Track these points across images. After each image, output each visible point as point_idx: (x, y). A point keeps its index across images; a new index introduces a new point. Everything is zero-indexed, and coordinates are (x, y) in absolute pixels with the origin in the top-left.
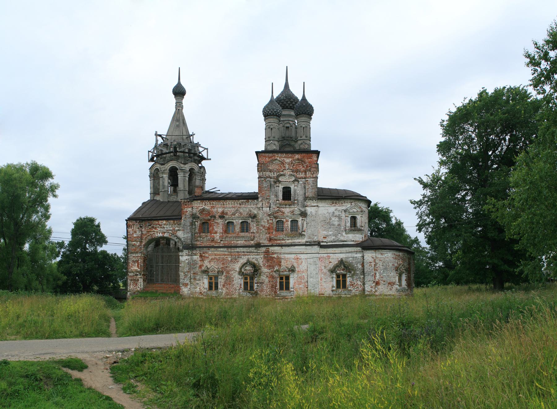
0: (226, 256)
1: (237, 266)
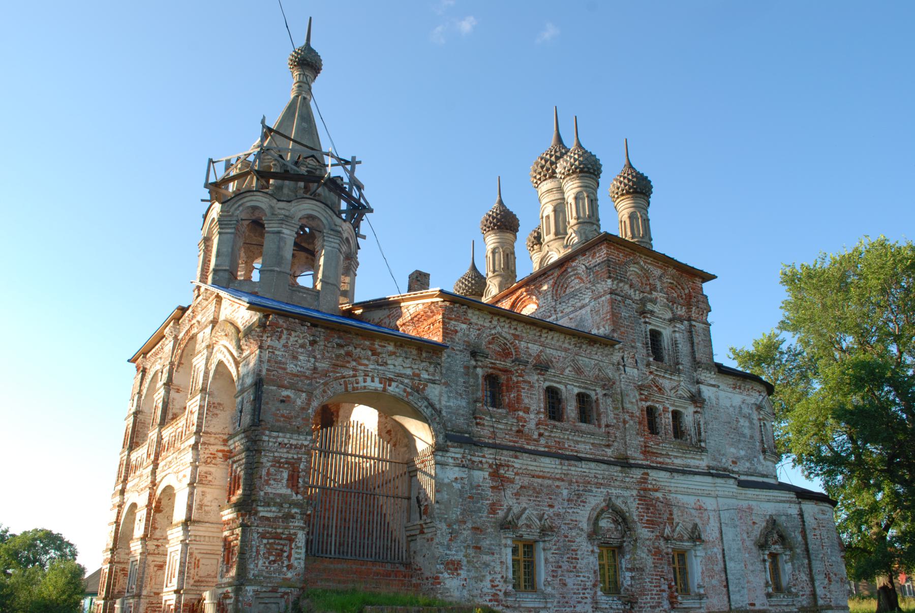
0: (557, 483)
1: (583, 516)
